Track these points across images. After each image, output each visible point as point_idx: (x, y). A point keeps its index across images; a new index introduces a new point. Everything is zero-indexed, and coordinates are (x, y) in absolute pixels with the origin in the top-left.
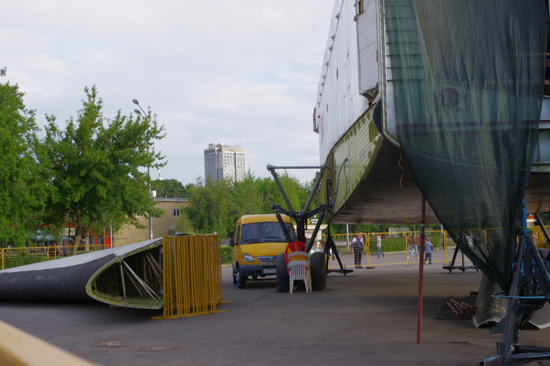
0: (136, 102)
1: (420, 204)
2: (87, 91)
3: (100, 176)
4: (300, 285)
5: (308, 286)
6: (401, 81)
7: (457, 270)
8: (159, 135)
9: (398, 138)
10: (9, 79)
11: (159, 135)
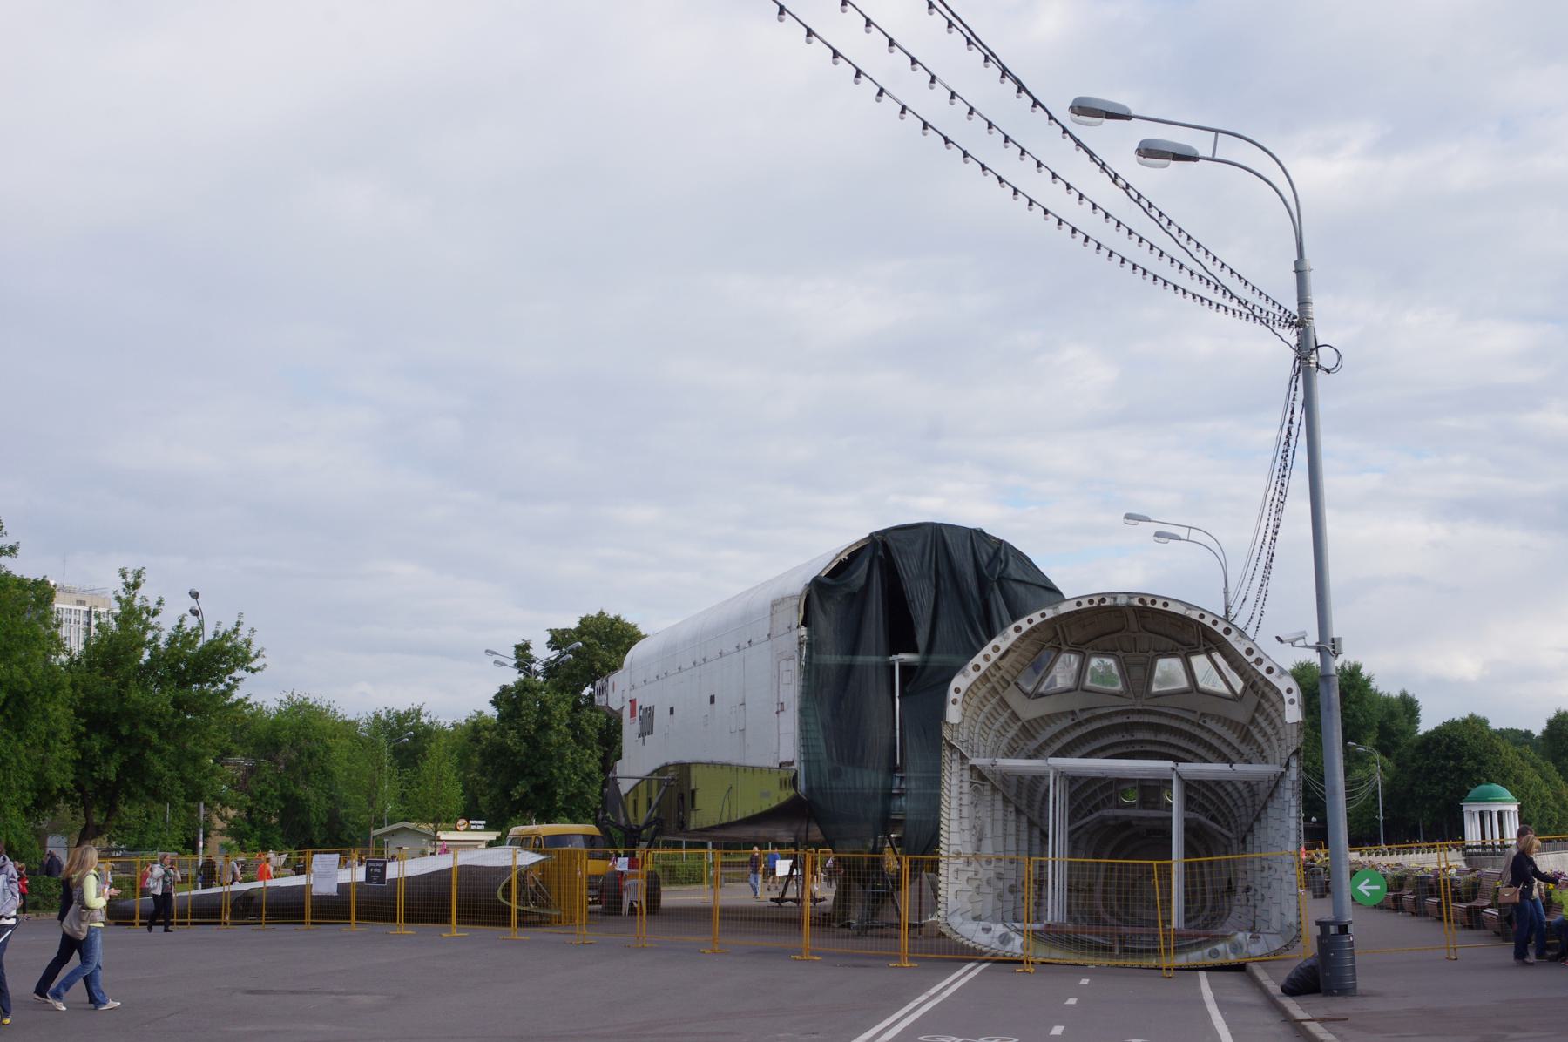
0: (195, 595)
2: (124, 576)
3: (154, 737)
8: (253, 665)
10: (23, 567)
11: (253, 665)
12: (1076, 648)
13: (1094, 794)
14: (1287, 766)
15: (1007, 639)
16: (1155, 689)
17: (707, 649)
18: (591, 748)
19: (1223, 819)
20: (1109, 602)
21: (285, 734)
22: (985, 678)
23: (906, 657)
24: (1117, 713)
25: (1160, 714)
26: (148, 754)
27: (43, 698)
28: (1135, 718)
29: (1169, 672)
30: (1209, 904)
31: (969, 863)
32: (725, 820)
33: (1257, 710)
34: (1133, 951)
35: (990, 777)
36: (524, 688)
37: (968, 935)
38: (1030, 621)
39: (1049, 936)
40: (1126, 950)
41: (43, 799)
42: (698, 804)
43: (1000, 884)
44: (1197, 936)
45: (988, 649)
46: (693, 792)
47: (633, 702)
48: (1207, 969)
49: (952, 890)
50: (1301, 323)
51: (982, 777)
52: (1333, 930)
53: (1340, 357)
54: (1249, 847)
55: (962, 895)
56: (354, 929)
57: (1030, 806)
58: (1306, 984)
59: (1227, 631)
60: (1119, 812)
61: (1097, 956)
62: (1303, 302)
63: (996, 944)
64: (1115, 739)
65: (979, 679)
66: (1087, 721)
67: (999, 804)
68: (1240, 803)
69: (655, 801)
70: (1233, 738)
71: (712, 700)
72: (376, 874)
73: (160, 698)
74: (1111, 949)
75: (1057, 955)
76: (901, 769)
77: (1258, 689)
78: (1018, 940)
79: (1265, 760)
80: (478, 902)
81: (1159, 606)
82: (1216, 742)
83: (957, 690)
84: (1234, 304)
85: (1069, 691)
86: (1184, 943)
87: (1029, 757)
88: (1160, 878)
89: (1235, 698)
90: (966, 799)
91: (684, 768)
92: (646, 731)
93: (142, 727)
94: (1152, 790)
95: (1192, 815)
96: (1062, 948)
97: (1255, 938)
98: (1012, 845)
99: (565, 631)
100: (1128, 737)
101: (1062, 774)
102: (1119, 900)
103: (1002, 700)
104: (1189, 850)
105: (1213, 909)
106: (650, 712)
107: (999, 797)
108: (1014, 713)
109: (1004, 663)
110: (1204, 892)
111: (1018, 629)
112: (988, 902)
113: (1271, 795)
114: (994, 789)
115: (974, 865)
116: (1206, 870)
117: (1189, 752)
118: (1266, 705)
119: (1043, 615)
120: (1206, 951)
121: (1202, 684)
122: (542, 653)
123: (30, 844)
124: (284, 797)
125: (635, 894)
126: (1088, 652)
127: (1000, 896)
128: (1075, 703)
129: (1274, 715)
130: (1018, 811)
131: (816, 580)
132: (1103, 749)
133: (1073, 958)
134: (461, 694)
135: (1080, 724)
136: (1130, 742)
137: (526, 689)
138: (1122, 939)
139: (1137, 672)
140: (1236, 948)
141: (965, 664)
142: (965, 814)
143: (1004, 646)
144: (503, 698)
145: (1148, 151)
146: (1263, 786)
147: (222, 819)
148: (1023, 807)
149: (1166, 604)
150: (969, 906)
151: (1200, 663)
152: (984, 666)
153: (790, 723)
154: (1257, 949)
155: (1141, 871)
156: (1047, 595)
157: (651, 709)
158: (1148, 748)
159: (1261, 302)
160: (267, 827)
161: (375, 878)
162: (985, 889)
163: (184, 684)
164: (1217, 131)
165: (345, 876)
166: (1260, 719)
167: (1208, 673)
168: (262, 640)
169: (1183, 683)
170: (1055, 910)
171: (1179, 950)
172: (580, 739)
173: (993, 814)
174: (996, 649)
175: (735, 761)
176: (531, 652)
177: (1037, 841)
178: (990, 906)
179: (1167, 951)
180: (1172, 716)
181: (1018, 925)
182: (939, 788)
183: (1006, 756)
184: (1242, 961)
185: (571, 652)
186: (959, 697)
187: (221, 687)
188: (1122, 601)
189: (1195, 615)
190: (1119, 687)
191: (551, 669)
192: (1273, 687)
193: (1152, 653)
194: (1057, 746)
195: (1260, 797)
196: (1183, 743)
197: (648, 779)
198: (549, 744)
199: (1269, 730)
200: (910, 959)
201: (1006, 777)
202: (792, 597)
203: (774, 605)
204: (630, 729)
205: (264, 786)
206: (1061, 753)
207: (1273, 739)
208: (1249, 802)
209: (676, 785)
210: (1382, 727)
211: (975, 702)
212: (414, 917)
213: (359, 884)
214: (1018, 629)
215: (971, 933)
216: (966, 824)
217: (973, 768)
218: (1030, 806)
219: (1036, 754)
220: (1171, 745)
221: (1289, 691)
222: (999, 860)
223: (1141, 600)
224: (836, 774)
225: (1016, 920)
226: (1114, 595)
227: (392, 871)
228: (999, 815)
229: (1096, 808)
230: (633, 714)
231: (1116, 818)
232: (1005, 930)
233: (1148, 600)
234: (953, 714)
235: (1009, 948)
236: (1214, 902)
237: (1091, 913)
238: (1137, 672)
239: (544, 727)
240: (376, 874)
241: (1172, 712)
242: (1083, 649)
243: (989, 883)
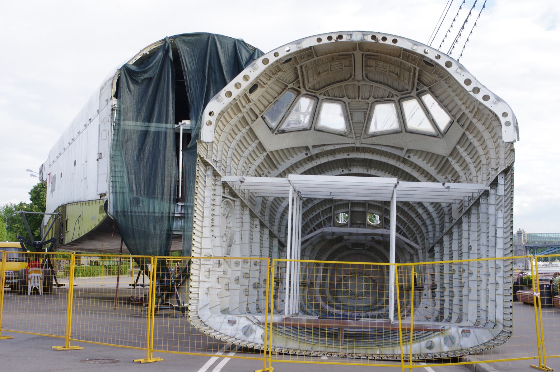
1: (120, 242)
4: (35, 291)
5: (41, 291)
6: (116, 192)
7: (140, 287)
9: (113, 217)
12: (313, 94)
13: (318, 216)
16: (372, 129)
24: (340, 151)
28: (353, 155)
31: (219, 264)
35: (240, 195)
37: (216, 327)
39: (288, 327)
43: (246, 282)
46: (67, 221)
49: (202, 291)
51: (233, 194)
57: (271, 222)
59: (449, 64)
63: (240, 335)
66: (318, 156)
67: (247, 218)
75: (293, 345)
78: (259, 332)
85: (305, 130)
89: (439, 134)
90: (218, 210)
103: (251, 129)
107: (247, 212)
108: (260, 144)
112: (235, 298)
114: (243, 205)
115: (224, 266)
120: (423, 343)
126: (321, 97)
128: (309, 140)
130: (262, 225)
131: (126, 69)
133: (305, 347)
135: (311, 159)
139: (358, 117)
140: (451, 340)
142: (216, 223)
146: (455, 207)
148: (266, 223)
149: (395, 41)
150: (218, 301)
152: (236, 93)
155: (346, 272)
162: (233, 286)
170: (291, 305)
173: (241, 225)
177: (276, 249)
178: (237, 300)
181: (259, 318)
186: (213, 119)
193: (372, 100)
211: (227, 129)
215: (220, 327)
216: (217, 232)
218: (271, 222)
222: (245, 262)
223: (374, 37)
224: (136, 202)
225: (259, 311)
226: (350, 34)
228: (247, 226)
229: (319, 226)
231: (333, 233)
232: (247, 323)
233: (380, 37)
235: (251, 338)
238: (358, 117)
241: (384, 149)
242: (319, 94)
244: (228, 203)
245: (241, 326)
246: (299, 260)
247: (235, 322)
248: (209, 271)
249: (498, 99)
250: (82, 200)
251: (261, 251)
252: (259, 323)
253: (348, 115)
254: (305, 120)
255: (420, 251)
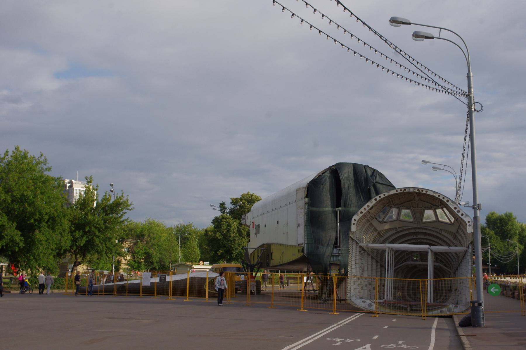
8: (130, 208)
11: (130, 208)
12: (397, 206)
14: (468, 247)
15: (372, 203)
16: (424, 220)
17: (278, 204)
18: (244, 238)
19: (447, 266)
20: (407, 190)
21: (146, 232)
22: (364, 216)
23: (340, 208)
24: (411, 229)
25: (426, 229)
26: (95, 238)
27: (60, 219)
28: (417, 231)
29: (429, 214)
30: (444, 294)
32: (281, 263)
33: (459, 228)
34: (415, 310)
36: (223, 218)
37: (357, 304)
38: (380, 197)
40: (412, 310)
41: (60, 254)
42: (273, 257)
43: (370, 286)
44: (437, 306)
45: (365, 206)
46: (272, 254)
47: (253, 223)
48: (439, 317)
49: (352, 288)
50: (468, 95)
52: (476, 304)
53: (482, 107)
54: (457, 275)
55: (355, 290)
56: (155, 298)
57: (381, 260)
58: (467, 323)
60: (412, 263)
61: (402, 312)
62: (469, 88)
63: (367, 307)
64: (394, 237)
65: (362, 216)
66: (401, 231)
67: (370, 259)
68: (454, 260)
69: (260, 255)
70: (451, 238)
71: (278, 222)
72: (163, 279)
73: (98, 219)
74: (407, 310)
75: (388, 311)
76: (339, 247)
77: (459, 222)
79: (461, 245)
80: (197, 288)
81: (424, 192)
82: (445, 239)
83: (355, 220)
84: (440, 88)
85: (394, 221)
86: (430, 308)
87: (381, 243)
88: (422, 285)
89: (451, 224)
90: (358, 257)
91: (269, 245)
92: (257, 233)
93: (93, 228)
94: (423, 255)
95: (437, 264)
96: (390, 309)
97: (456, 307)
98: (374, 273)
99: (237, 199)
100: (415, 237)
101: (392, 249)
102: (413, 293)
103: (371, 223)
104: (436, 275)
105: (446, 296)
106: (258, 226)
107: (370, 257)
109: (372, 211)
110: (442, 290)
111: (376, 200)
113: (463, 258)
114: (368, 254)
116: (443, 283)
117: (436, 242)
118: (462, 227)
119: (384, 195)
120: (439, 311)
121: (440, 219)
122: (229, 206)
123: (56, 268)
124: (145, 253)
125: (251, 287)
127: (370, 290)
129: (464, 230)
130: (377, 262)
132: (406, 241)
133: (393, 312)
134: (203, 220)
135: (398, 232)
136: (416, 239)
137: (223, 218)
138: (411, 306)
140: (450, 310)
141: (358, 211)
142: (357, 262)
143: (371, 206)
144: (217, 222)
145: (417, 36)
147: (125, 260)
148: (379, 260)
149: (427, 192)
150: (358, 294)
151: (439, 211)
152: (364, 212)
153: (302, 230)
154: (457, 310)
156: (392, 188)
157: (259, 225)
158: (422, 241)
159: (452, 87)
160: (140, 263)
161: (162, 280)
163: (107, 214)
164: (441, 28)
165: (153, 280)
166: (460, 231)
167: (443, 215)
168: (132, 199)
169: (434, 219)
170: (389, 296)
171: (428, 310)
172: (240, 234)
174: (368, 206)
175: (284, 242)
176: (225, 206)
179: (424, 310)
180: (430, 230)
182: (348, 253)
183: (373, 243)
184: (451, 314)
185: (238, 206)
186: (355, 222)
187: (119, 215)
188: (411, 190)
189: (436, 195)
190: (412, 220)
191: (232, 212)
192: (464, 221)
193: (423, 208)
194: (391, 240)
195: (460, 258)
196: (434, 239)
197: (257, 249)
198: (230, 237)
199: (463, 235)
200: (337, 311)
201: (372, 250)
202: (303, 188)
203: (297, 190)
204: (252, 232)
205: (139, 249)
206: (392, 242)
207: (464, 238)
208: (457, 260)
209: (266, 251)
210: (520, 234)
211: (361, 224)
212: (175, 294)
213: (157, 283)
214: (376, 200)
216: (358, 266)
217: (360, 247)
218: (381, 260)
219: (383, 242)
220: (430, 240)
221: (469, 222)
222: (370, 278)
223: (418, 190)
226: (409, 188)
227: (168, 279)
228: (370, 263)
229: (405, 261)
230: (253, 227)
231: (412, 264)
233: (421, 190)
234: (353, 228)
235: (371, 308)
236: (443, 294)
237: (403, 297)
239: (228, 231)
240: (163, 279)
242: (400, 206)
243: (366, 286)
244: (362, 254)
245: (367, 303)
246: (155, 297)
247: (365, 302)
248: (354, 282)
249: (467, 215)
250: (284, 243)
251: (376, 273)
252: (374, 302)
253: (414, 214)
254: (394, 217)
255: (452, 273)
